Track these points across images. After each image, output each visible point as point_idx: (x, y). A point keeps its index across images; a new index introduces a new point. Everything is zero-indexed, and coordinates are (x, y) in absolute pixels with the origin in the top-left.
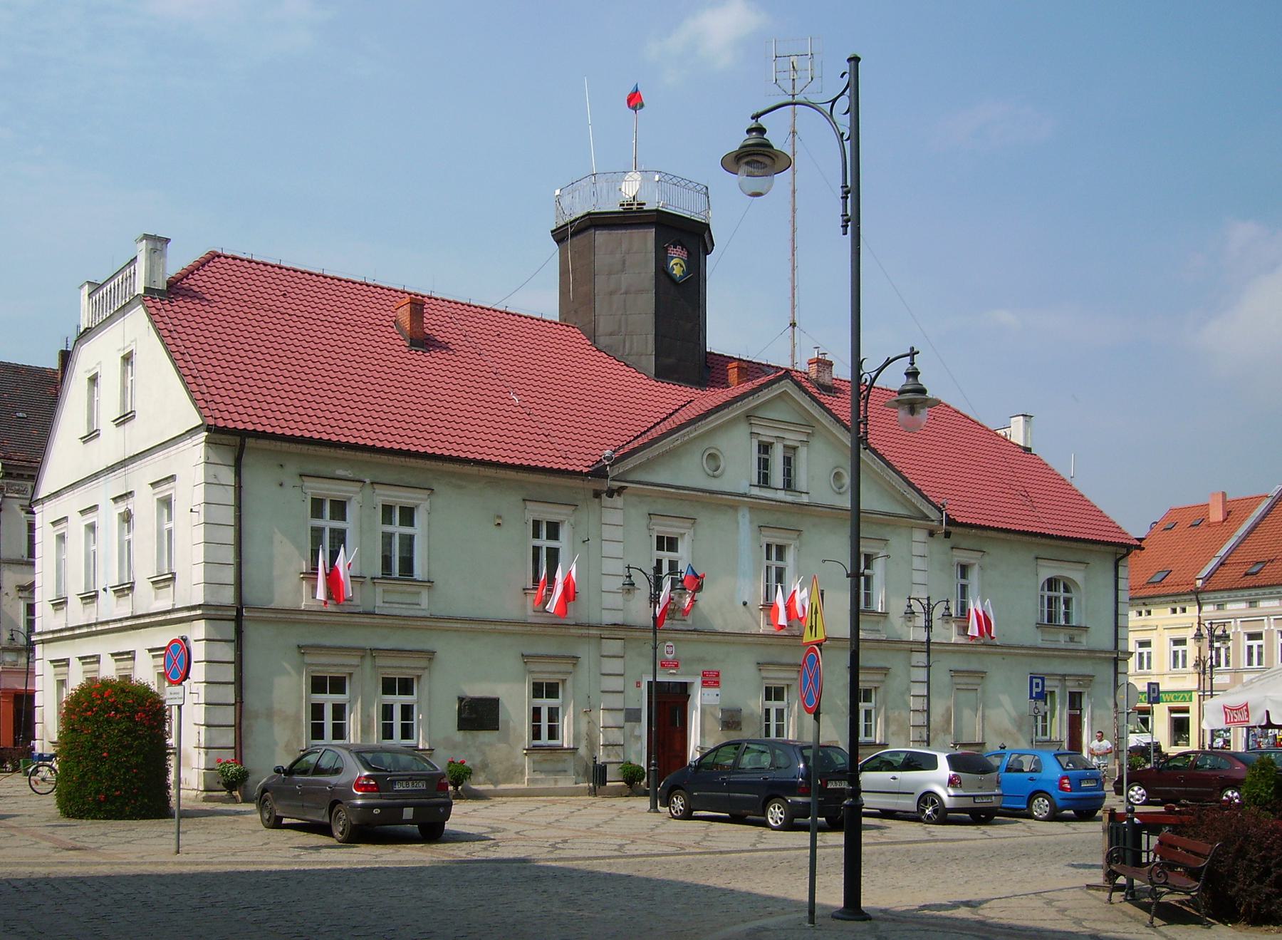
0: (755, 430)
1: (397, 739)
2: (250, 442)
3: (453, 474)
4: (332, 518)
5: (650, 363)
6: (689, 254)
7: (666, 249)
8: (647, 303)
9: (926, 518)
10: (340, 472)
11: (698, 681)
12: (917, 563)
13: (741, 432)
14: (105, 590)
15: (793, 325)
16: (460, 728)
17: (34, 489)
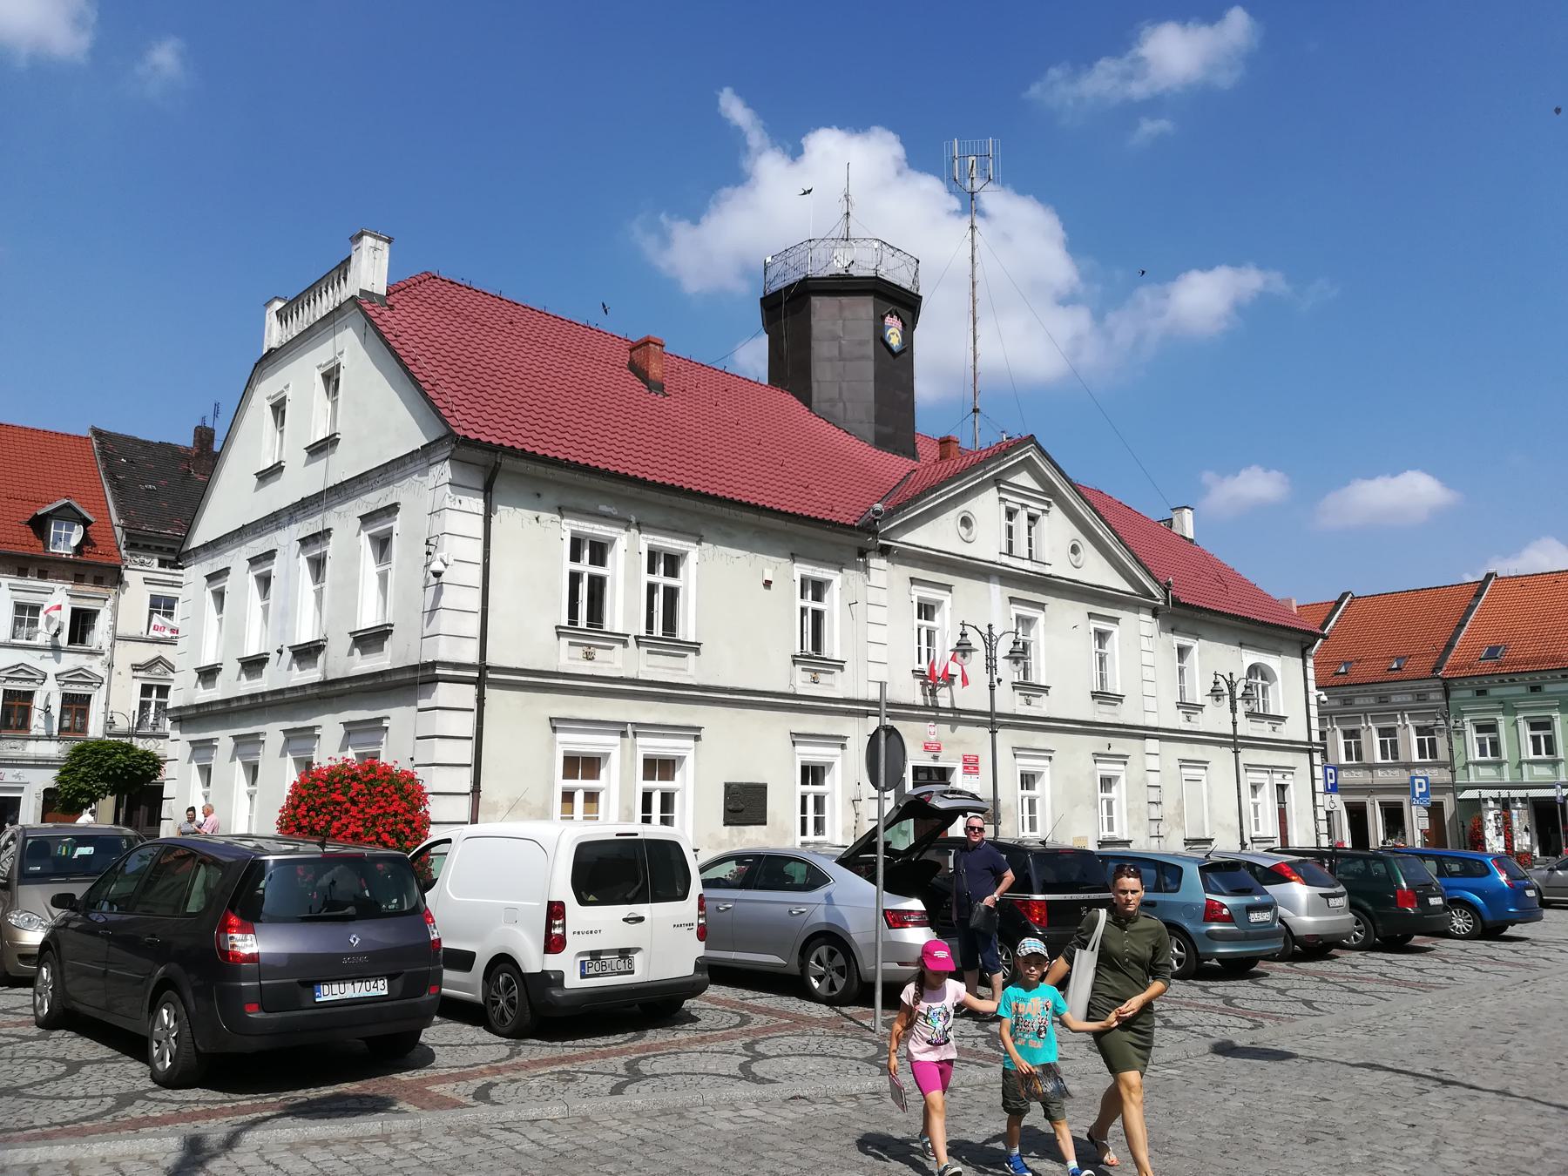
0: (1003, 495)
1: (811, 836)
2: (507, 462)
3: (722, 520)
4: (592, 562)
5: (869, 430)
6: (904, 325)
7: (883, 318)
8: (869, 368)
9: (1152, 596)
10: (603, 508)
11: (959, 767)
12: (1145, 643)
13: (992, 494)
14: (280, 652)
15: (976, 411)
16: (726, 824)
17: (189, 527)
